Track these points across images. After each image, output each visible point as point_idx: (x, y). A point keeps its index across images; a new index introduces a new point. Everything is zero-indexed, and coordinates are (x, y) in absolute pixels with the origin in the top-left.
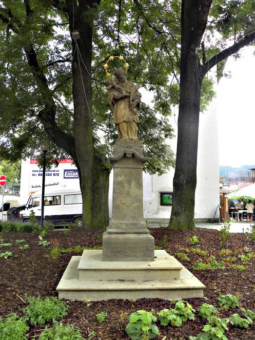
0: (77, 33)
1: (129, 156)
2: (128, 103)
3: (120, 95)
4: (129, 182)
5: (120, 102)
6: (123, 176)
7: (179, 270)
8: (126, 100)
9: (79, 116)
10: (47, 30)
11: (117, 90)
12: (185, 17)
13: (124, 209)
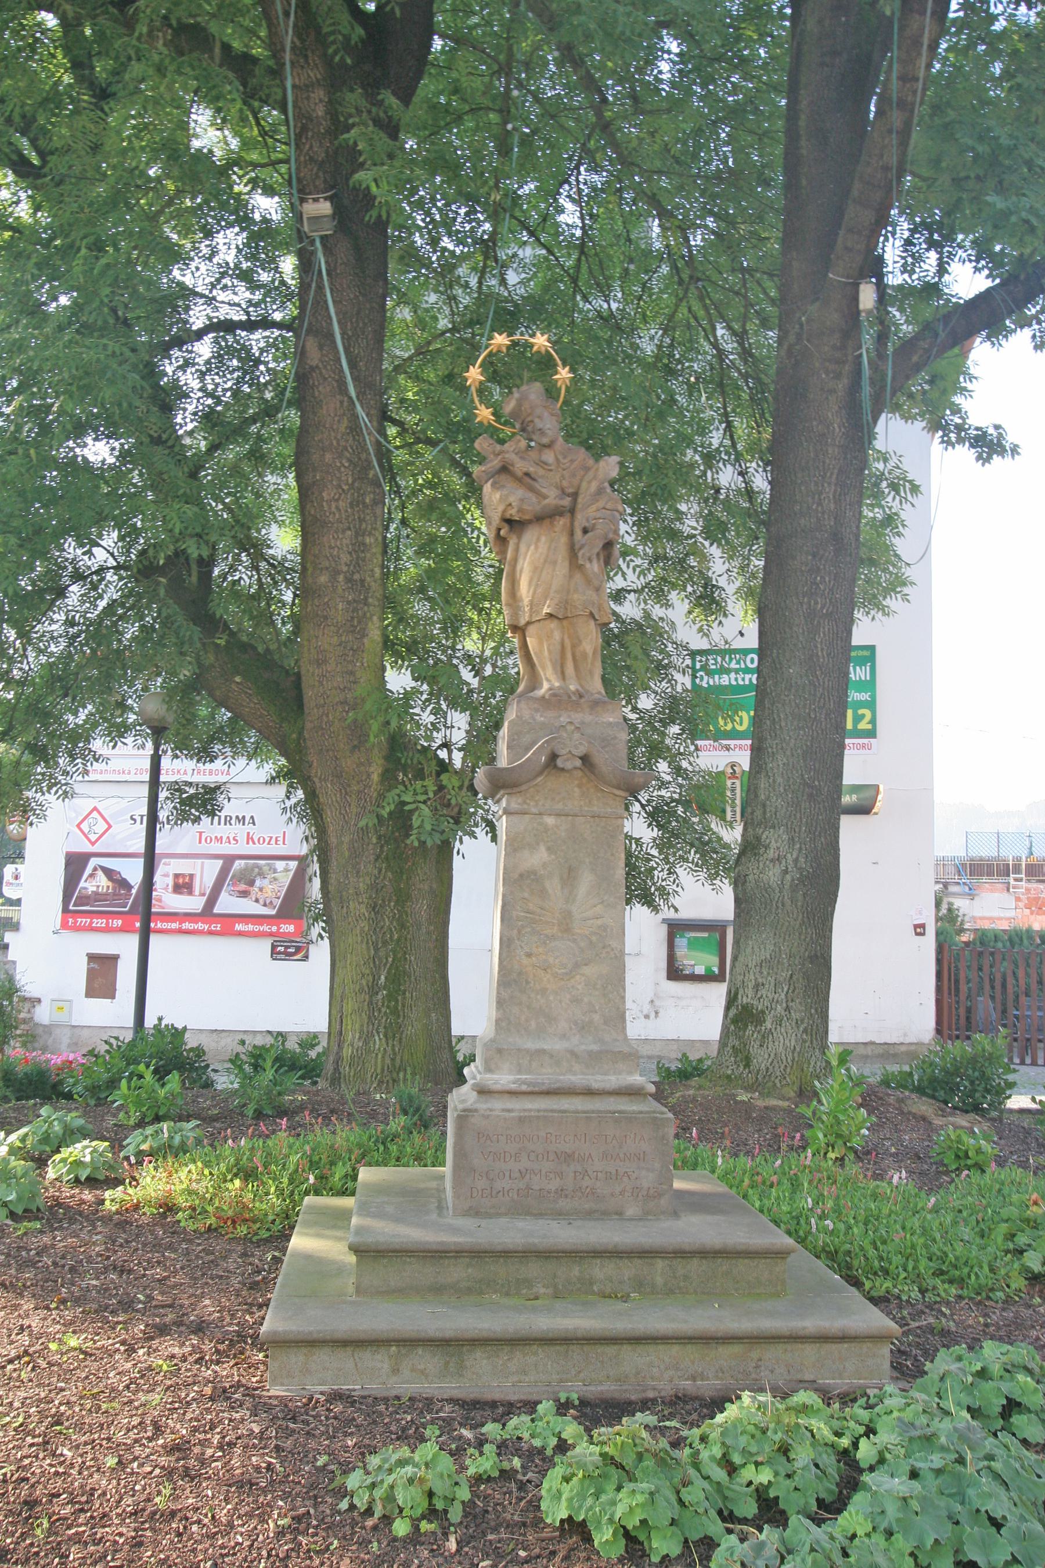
0: (325, 208)
1: (569, 765)
2: (564, 539)
3: (533, 505)
4: (569, 877)
5: (530, 534)
6: (542, 848)
7: (780, 1254)
8: (561, 522)
9: (323, 579)
10: (282, 307)
11: (519, 480)
12: (806, 147)
13: (544, 991)
